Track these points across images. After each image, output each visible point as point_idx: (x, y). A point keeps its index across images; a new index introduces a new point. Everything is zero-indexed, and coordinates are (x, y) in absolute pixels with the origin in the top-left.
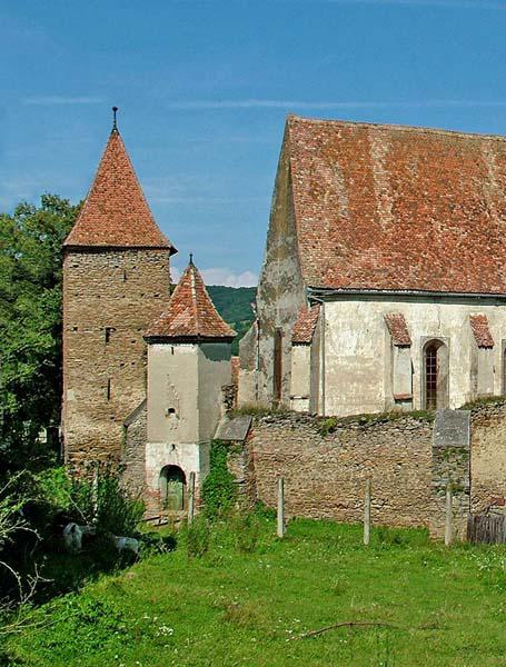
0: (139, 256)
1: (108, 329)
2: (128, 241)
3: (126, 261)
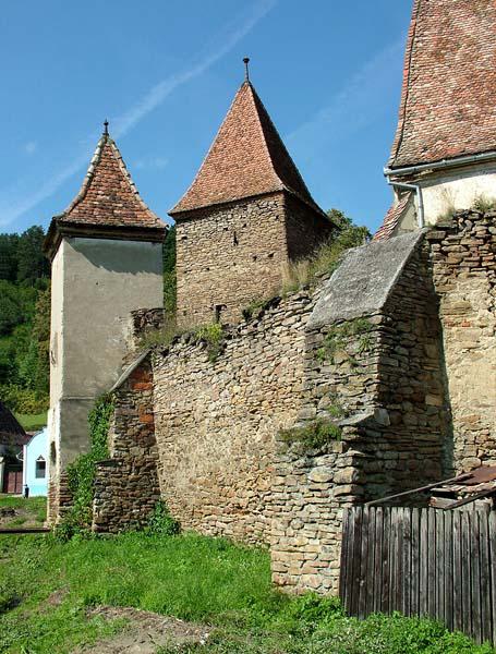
0: (249, 210)
1: (219, 308)
2: (239, 193)
3: (235, 219)
